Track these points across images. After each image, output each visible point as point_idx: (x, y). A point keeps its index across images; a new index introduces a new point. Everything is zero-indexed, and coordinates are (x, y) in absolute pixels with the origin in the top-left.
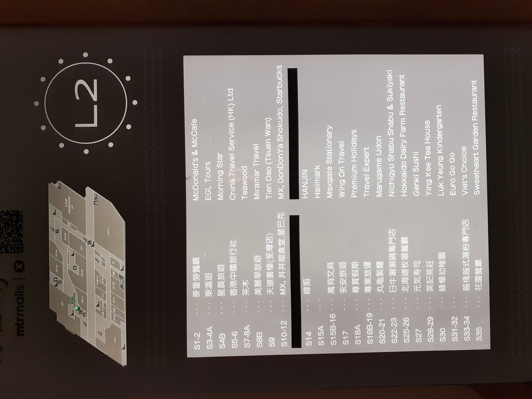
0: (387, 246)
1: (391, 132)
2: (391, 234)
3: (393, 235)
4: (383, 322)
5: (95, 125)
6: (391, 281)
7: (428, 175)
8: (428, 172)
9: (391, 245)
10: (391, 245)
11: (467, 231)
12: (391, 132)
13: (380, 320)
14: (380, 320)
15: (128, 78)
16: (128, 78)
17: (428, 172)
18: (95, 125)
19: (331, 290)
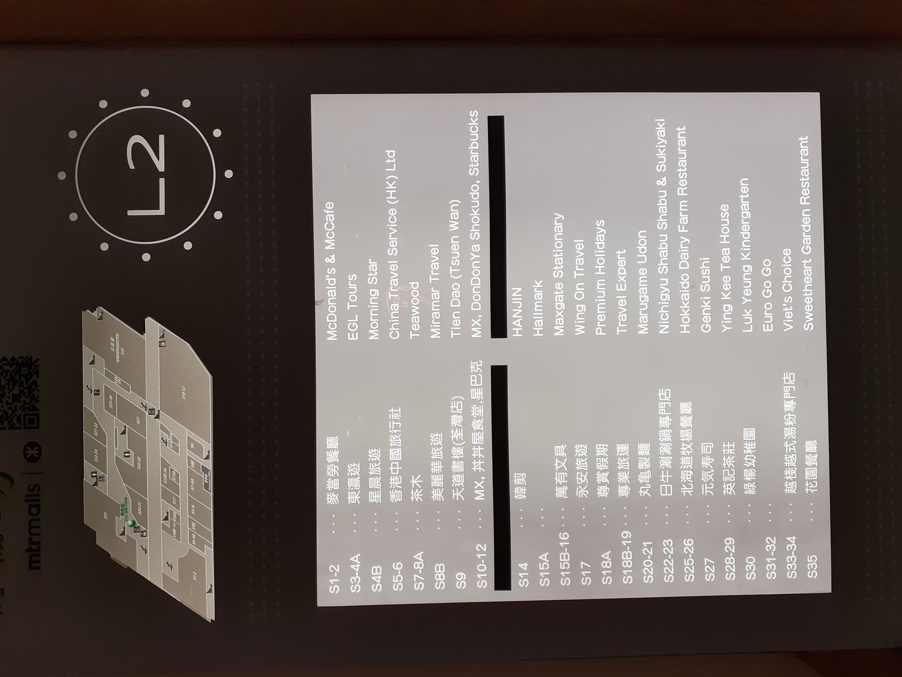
0: (657, 417)
2: (663, 397)
3: (666, 398)
4: (649, 546)
5: (161, 211)
6: (663, 476)
7: (726, 297)
8: (726, 292)
9: (663, 416)
10: (663, 416)
11: (792, 392)
13: (644, 544)
14: (644, 544)
15: (217, 133)
16: (217, 133)
17: (726, 292)
18: (161, 211)
19: (561, 492)
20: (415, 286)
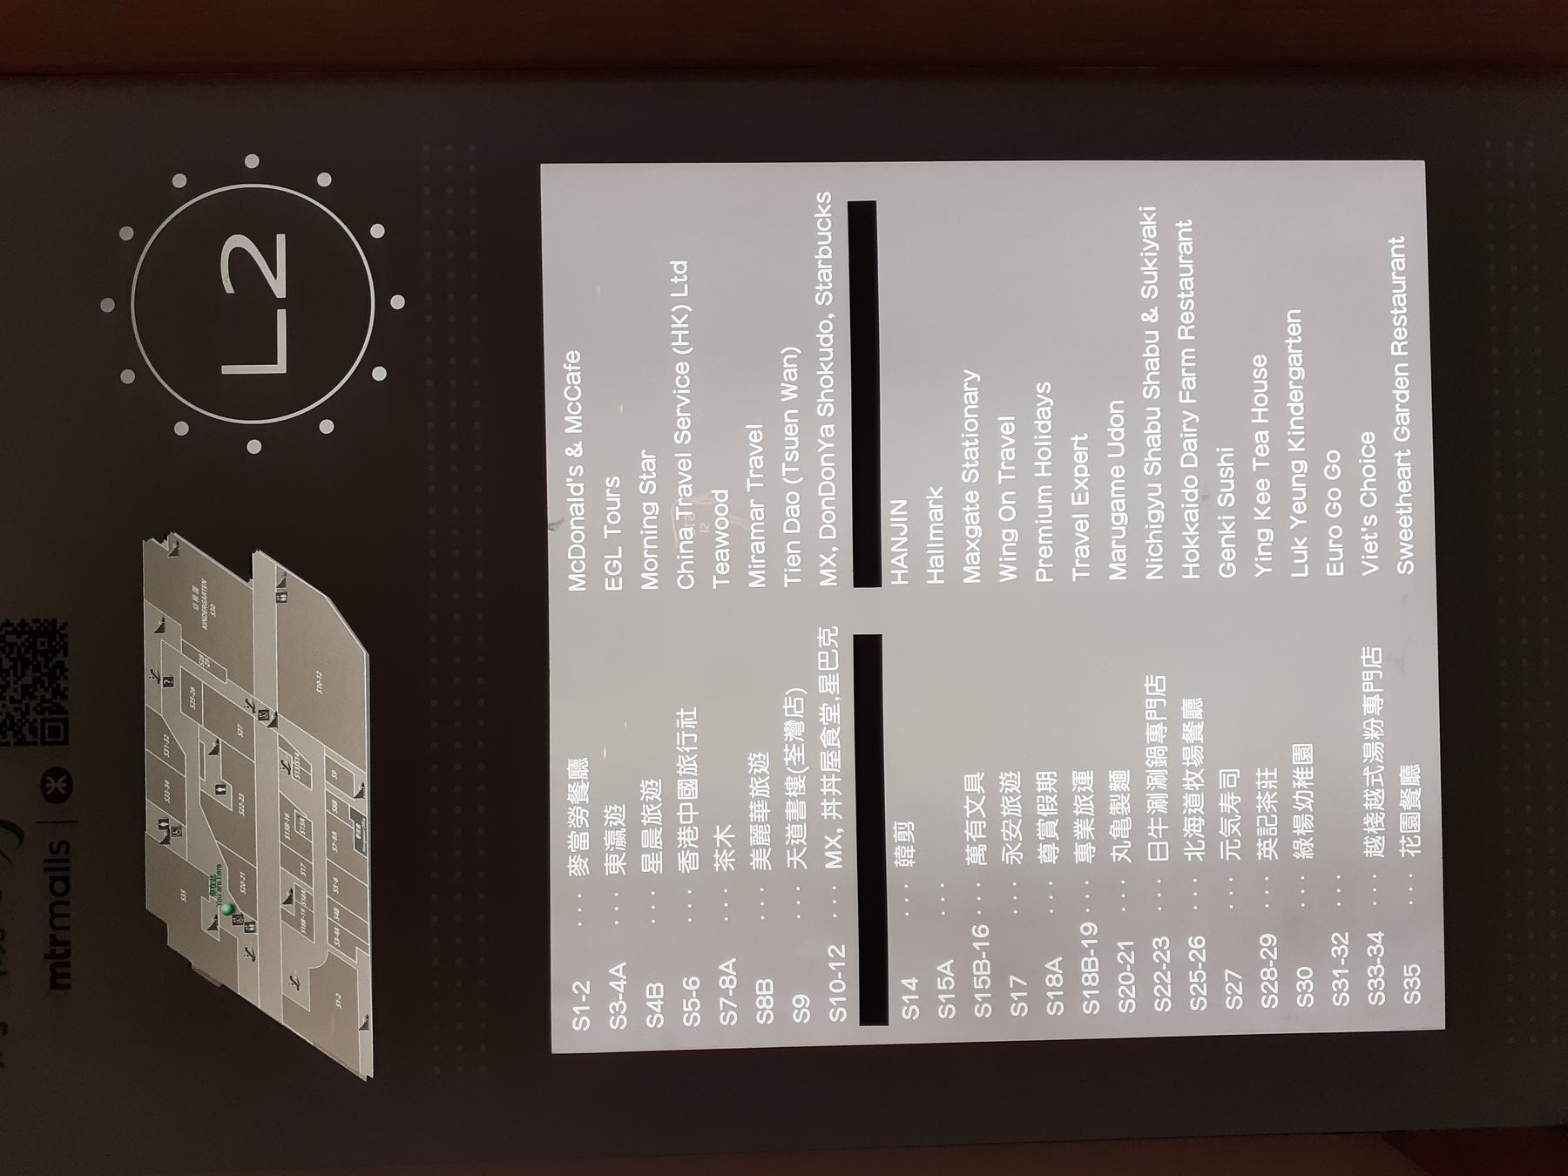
0: (1142, 724)
1: (1151, 389)
2: (1152, 689)
3: (1158, 692)
4: (1128, 949)
9: (1152, 722)
10: (1152, 722)
12: (1151, 389)
13: (1120, 944)
14: (1120, 944)
20: (721, 496)
